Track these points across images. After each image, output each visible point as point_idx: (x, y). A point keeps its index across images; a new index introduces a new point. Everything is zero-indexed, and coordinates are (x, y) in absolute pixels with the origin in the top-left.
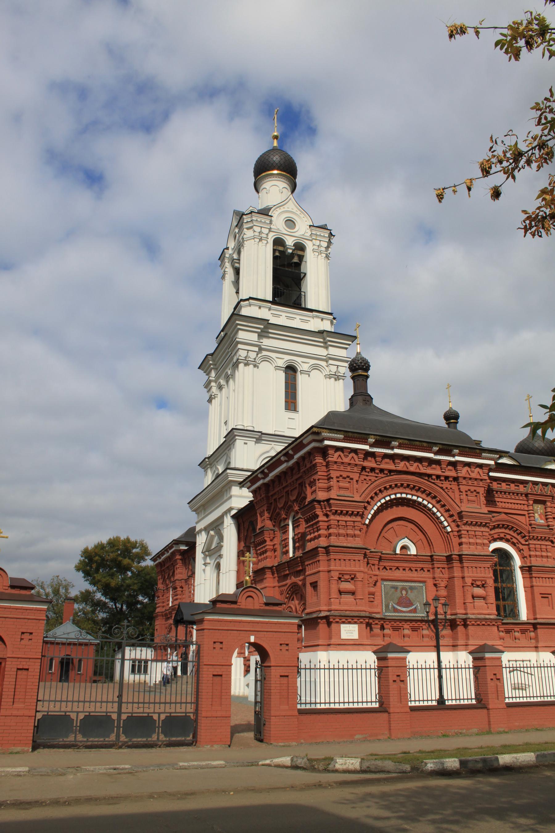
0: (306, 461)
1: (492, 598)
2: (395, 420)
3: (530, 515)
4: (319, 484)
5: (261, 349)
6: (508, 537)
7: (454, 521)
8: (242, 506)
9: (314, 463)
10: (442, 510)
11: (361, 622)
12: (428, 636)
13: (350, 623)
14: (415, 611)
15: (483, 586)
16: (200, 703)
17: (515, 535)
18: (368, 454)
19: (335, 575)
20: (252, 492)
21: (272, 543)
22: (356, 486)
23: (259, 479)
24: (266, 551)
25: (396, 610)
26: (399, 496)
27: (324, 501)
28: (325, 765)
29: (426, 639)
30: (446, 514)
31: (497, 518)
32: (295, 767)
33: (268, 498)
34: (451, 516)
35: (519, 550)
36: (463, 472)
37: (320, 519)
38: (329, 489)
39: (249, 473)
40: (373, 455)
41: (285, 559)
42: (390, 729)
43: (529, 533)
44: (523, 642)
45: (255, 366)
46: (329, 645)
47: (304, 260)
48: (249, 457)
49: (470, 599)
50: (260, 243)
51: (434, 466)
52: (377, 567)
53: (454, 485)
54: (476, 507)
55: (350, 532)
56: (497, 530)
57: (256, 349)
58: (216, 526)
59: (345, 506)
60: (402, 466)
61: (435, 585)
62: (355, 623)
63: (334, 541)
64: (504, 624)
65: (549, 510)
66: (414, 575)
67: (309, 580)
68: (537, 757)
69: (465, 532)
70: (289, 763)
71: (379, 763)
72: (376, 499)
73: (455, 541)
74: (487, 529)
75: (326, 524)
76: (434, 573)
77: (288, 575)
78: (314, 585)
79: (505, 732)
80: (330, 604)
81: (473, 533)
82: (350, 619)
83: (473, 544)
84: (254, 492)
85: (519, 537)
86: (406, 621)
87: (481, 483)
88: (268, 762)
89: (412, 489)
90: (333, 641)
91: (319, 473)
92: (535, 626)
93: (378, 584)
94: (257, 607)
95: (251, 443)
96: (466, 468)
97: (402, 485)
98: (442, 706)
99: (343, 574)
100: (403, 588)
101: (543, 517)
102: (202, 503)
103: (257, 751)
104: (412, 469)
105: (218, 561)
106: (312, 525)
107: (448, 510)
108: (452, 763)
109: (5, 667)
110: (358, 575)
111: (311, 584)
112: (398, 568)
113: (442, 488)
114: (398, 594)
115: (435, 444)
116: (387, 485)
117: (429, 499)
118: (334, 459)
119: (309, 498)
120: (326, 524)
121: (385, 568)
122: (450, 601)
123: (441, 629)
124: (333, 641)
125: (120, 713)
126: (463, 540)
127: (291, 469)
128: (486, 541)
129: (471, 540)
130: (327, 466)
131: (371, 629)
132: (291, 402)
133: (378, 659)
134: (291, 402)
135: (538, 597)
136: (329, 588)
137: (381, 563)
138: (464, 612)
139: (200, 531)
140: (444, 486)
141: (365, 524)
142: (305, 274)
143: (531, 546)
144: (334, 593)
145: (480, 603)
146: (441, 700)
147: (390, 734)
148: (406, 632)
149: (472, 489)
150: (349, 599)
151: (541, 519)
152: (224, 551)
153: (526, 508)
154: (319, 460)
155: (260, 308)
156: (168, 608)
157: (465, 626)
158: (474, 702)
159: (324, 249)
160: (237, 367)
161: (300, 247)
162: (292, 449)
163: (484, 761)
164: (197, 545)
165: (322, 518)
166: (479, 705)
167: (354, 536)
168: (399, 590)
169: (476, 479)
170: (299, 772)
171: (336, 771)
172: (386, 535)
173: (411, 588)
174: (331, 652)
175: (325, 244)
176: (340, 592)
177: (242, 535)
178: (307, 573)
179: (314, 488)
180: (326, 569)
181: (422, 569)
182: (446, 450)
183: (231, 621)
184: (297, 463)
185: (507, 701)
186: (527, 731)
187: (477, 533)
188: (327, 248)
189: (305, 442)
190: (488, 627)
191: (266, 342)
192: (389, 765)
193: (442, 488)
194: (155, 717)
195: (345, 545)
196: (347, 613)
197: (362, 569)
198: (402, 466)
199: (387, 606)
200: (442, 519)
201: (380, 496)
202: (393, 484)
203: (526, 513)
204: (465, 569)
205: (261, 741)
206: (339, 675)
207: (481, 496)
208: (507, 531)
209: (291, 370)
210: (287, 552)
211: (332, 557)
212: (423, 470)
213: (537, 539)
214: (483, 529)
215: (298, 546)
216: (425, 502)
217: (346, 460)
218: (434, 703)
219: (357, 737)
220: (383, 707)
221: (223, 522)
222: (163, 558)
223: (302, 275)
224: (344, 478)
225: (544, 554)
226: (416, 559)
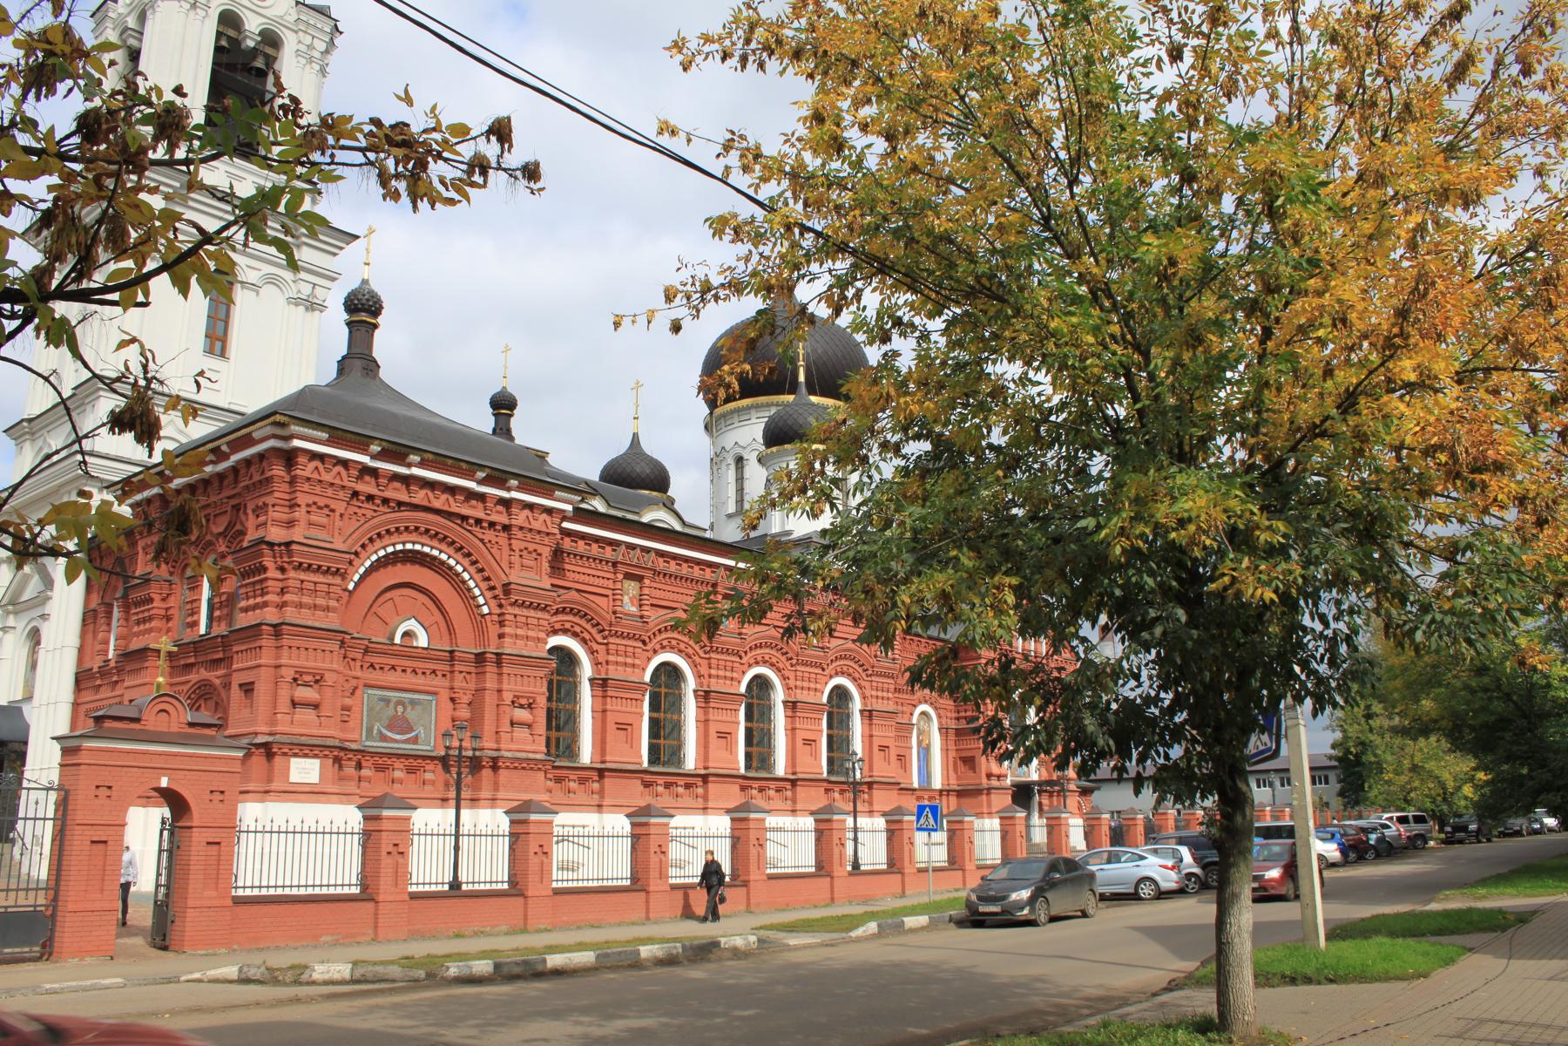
0: (252, 469)
1: (541, 728)
3: (616, 596)
4: (274, 514)
6: (578, 629)
7: (495, 597)
9: (269, 474)
10: (478, 577)
12: (433, 783)
13: (306, 756)
14: (415, 740)
15: (530, 706)
17: (588, 627)
19: (289, 674)
21: (164, 605)
22: (338, 523)
24: (150, 619)
25: (384, 738)
26: (409, 546)
27: (280, 545)
28: (298, 974)
29: (428, 788)
30: (484, 585)
31: (564, 597)
32: (245, 981)
34: (492, 588)
35: (592, 652)
36: (520, 518)
37: (269, 575)
38: (290, 524)
40: (374, 472)
41: (189, 636)
42: (376, 927)
44: (581, 797)
46: (267, 792)
49: (506, 727)
50: (192, 13)
51: (474, 502)
52: (359, 664)
53: (502, 538)
54: (533, 577)
55: (320, 601)
56: (561, 617)
59: (317, 557)
60: (420, 496)
61: (452, 700)
62: (316, 756)
63: (290, 614)
64: (555, 768)
65: (646, 591)
66: (420, 681)
67: (237, 679)
68: (598, 957)
70: (235, 976)
71: (380, 969)
72: (370, 548)
73: (494, 630)
74: (547, 616)
75: (280, 585)
76: (452, 680)
77: (192, 665)
78: (248, 688)
79: (547, 930)
80: (273, 723)
82: (306, 749)
83: (522, 637)
85: (594, 631)
86: (399, 756)
87: (546, 540)
88: (197, 975)
89: (432, 537)
90: (275, 786)
91: (277, 495)
92: (601, 773)
93: (358, 692)
94: (174, 728)
96: (527, 512)
97: (417, 529)
98: (453, 893)
99: (301, 674)
100: (400, 702)
103: (166, 963)
104: (437, 504)
105: (33, 624)
106: (254, 583)
108: (483, 967)
110: (327, 675)
111: (241, 685)
112: (393, 668)
113: (482, 540)
114: (390, 711)
115: (482, 467)
116: (392, 528)
117: (459, 556)
118: (307, 474)
119: (252, 535)
120: (280, 585)
122: (474, 724)
123: (464, 772)
124: (275, 786)
126: (507, 630)
127: (221, 476)
128: (542, 635)
129: (519, 632)
130: (292, 482)
131: (341, 767)
133: (366, 818)
135: (611, 727)
136: (275, 695)
137: (367, 658)
138: (495, 746)
141: (346, 590)
144: (284, 705)
146: (455, 885)
147: (376, 934)
148: (398, 774)
149: (531, 547)
150: (308, 715)
152: (52, 608)
153: (610, 584)
154: (278, 471)
157: (495, 768)
158: (506, 886)
159: (317, 54)
162: (228, 443)
163: (526, 963)
165: (272, 573)
166: (514, 891)
168: (392, 705)
170: (252, 987)
171: (314, 983)
172: (380, 611)
173: (413, 703)
174: (270, 804)
175: (322, 46)
176: (294, 704)
178: (235, 666)
179: (262, 519)
180: (272, 662)
181: (434, 672)
182: (497, 478)
183: (128, 752)
184: (235, 469)
185: (554, 885)
186: (579, 928)
188: (327, 52)
189: (256, 435)
192: (395, 971)
193: (482, 540)
195: (309, 623)
196: (304, 740)
197: (335, 666)
198: (420, 496)
199: (370, 730)
200: (477, 592)
201: (378, 544)
202: (402, 526)
203: (609, 593)
204: (505, 677)
205: (165, 948)
206: (295, 839)
208: (577, 619)
210: (196, 624)
211: (285, 642)
212: (455, 508)
213: (622, 636)
214: (540, 614)
215: (219, 618)
216: (452, 562)
217: (327, 477)
219: (324, 939)
220: (368, 892)
224: (320, 508)
225: (629, 660)
226: (426, 654)
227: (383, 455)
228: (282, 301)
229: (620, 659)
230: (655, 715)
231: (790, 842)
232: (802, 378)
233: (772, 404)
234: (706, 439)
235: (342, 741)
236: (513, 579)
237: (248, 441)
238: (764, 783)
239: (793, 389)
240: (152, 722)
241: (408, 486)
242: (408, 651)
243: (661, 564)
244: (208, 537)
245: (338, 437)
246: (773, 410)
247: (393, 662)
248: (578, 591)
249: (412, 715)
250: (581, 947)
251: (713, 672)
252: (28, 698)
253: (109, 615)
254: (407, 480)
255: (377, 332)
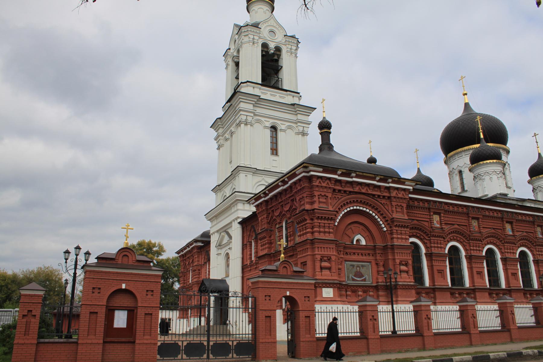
0: (297, 185)
1: (411, 273)
2: (351, 161)
5: (255, 115)
8: (246, 216)
11: (335, 287)
13: (328, 287)
14: (365, 280)
16: (257, 334)
18: (337, 181)
19: (318, 257)
20: (255, 206)
23: (262, 198)
25: (353, 280)
26: (355, 208)
27: (310, 210)
33: (267, 210)
35: (424, 243)
37: (308, 222)
38: (312, 203)
39: (253, 195)
43: (431, 232)
45: (251, 125)
47: (281, 57)
48: (252, 185)
51: (376, 189)
52: (342, 252)
55: (327, 230)
57: (252, 115)
58: (225, 230)
60: (357, 189)
61: (377, 264)
62: (331, 287)
63: (317, 235)
65: (442, 218)
66: (364, 258)
69: (395, 231)
73: (389, 237)
76: (376, 256)
81: (400, 232)
82: (328, 285)
84: (257, 206)
86: (360, 286)
90: (318, 299)
93: (343, 263)
95: (250, 176)
98: (394, 335)
99: (323, 257)
100: (358, 266)
101: (439, 223)
102: (213, 216)
106: (302, 226)
107: (385, 217)
109: (137, 313)
110: (332, 257)
112: (354, 253)
113: (381, 203)
114: (355, 270)
121: (347, 253)
125: (208, 341)
127: (285, 190)
129: (399, 236)
132: (274, 151)
134: (274, 151)
139: (214, 233)
140: (382, 202)
141: (335, 225)
142: (282, 67)
143: (432, 241)
144: (318, 269)
145: (404, 275)
146: (394, 332)
148: (360, 293)
149: (399, 204)
150: (326, 272)
151: (438, 224)
155: (254, 88)
156: (188, 284)
160: (240, 126)
161: (278, 49)
162: (287, 178)
164: (211, 242)
167: (329, 233)
168: (355, 267)
169: (401, 198)
172: (347, 233)
173: (363, 266)
175: (294, 48)
177: (245, 234)
184: (290, 187)
187: (402, 232)
190: (410, 290)
191: (259, 110)
193: (381, 203)
194: (231, 343)
195: (324, 238)
196: (326, 281)
197: (334, 253)
199: (348, 277)
207: (405, 209)
209: (274, 128)
213: (435, 236)
218: (390, 333)
221: (232, 226)
222: (185, 251)
223: (280, 68)
224: (323, 196)
225: (439, 245)
226: (365, 248)
227: (342, 175)
228: (293, 134)
229: (436, 245)
230: (451, 266)
231: (487, 316)
232: (482, 136)
233: (470, 149)
234: (446, 167)
235: (340, 281)
236: (394, 216)
237: (295, 175)
238: (498, 292)
239: (479, 141)
240: (282, 272)
241: (352, 185)
242: (358, 246)
243: (446, 208)
244: (283, 213)
245: (326, 170)
246: (471, 152)
247: (354, 251)
248: (417, 220)
249: (363, 271)
250: (465, 354)
251: (472, 248)
252: (227, 276)
253: (251, 245)
254: (352, 183)
255: (331, 135)
